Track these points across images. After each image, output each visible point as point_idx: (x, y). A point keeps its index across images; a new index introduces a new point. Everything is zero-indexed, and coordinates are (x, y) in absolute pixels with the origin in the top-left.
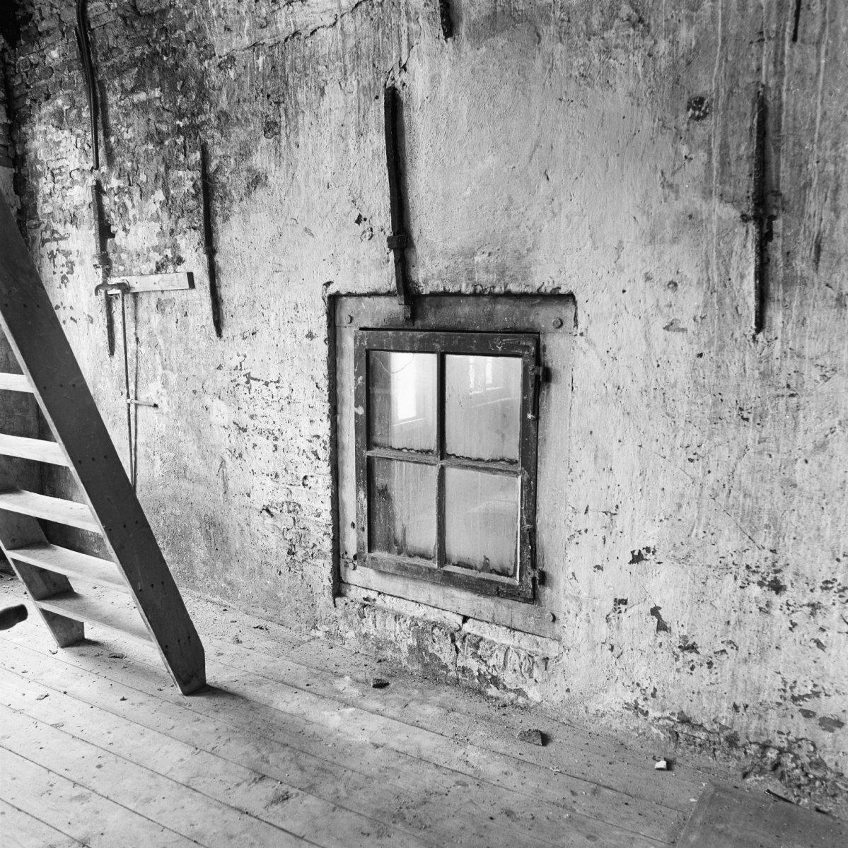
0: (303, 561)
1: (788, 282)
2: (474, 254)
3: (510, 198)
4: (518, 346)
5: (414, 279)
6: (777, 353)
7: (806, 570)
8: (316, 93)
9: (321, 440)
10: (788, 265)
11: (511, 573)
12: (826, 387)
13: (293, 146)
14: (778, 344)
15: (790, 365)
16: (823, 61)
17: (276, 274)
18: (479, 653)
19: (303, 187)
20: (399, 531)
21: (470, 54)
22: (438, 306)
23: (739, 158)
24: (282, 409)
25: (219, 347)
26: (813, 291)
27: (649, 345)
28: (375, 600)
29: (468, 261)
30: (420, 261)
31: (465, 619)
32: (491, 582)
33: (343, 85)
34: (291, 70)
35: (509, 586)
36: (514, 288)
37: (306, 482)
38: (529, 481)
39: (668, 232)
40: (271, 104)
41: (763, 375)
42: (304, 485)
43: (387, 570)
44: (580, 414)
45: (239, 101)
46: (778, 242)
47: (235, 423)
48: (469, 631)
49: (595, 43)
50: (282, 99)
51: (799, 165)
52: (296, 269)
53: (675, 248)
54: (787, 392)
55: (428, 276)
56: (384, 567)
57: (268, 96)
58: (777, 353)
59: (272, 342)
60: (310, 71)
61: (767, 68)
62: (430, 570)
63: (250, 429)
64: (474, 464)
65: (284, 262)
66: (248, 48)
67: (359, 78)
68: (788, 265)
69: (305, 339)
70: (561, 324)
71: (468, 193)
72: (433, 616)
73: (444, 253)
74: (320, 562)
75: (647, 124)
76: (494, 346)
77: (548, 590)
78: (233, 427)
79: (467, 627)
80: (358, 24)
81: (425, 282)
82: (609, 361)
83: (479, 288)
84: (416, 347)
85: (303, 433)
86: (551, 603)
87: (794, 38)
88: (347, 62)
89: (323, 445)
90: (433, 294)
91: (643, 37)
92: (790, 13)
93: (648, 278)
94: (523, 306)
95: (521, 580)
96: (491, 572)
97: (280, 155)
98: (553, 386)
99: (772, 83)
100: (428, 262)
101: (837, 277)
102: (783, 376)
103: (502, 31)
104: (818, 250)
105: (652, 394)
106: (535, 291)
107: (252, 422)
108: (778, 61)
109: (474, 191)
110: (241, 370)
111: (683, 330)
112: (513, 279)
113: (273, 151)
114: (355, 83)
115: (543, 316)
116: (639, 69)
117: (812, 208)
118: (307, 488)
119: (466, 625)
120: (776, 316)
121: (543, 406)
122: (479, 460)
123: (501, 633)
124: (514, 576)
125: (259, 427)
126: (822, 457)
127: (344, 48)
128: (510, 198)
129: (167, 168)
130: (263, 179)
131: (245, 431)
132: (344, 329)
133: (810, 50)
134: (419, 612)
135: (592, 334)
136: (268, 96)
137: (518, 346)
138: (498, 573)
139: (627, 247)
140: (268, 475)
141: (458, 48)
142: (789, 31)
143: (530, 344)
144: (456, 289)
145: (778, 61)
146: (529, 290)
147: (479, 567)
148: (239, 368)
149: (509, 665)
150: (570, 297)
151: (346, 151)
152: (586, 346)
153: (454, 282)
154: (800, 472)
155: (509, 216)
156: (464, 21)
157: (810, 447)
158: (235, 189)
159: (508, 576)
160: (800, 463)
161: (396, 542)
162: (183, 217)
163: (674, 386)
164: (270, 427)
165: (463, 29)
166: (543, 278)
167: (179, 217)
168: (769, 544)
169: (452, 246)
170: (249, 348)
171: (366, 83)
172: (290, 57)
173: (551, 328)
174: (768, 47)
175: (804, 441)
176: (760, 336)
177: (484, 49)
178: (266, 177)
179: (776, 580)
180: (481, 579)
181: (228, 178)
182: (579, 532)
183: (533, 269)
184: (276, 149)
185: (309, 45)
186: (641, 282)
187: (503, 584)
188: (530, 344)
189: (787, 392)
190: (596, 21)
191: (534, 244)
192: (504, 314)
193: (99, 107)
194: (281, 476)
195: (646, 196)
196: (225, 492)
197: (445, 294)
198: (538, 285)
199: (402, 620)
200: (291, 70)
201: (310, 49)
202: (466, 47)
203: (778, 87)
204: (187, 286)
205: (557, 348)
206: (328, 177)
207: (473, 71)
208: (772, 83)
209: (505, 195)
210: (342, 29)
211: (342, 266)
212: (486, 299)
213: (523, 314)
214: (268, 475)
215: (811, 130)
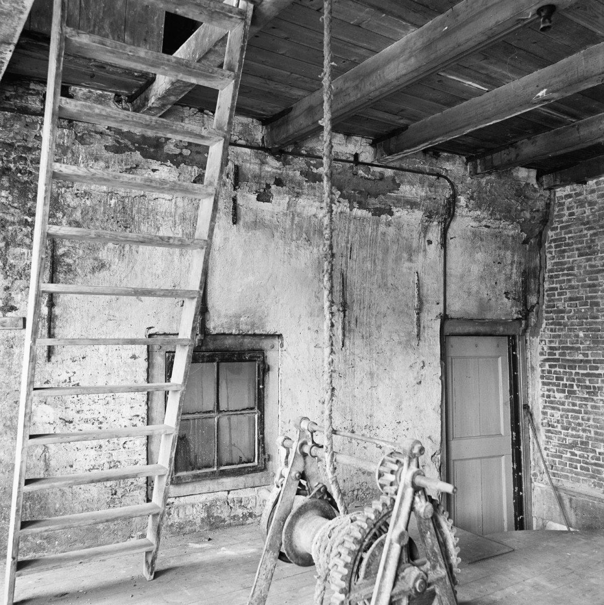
0: (122, 496)
1: (350, 331)
2: (241, 317)
3: (259, 295)
4: (256, 357)
5: (208, 326)
6: (348, 354)
7: (360, 424)
8: (155, 229)
9: (140, 418)
10: (349, 326)
11: (252, 461)
12: (361, 363)
13: (134, 252)
14: (348, 351)
15: (351, 357)
16: (121, 51)
17: (109, 322)
18: (242, 504)
19: (139, 275)
20: (192, 457)
21: (244, 234)
22: (215, 340)
23: (337, 291)
24: (108, 403)
25: (47, 368)
26: (356, 334)
27: (309, 353)
28: (173, 503)
29: (237, 319)
30: (212, 318)
31: (229, 492)
32: (244, 468)
33: (173, 229)
34: (138, 213)
35: (253, 467)
36: (257, 332)
37: (125, 445)
38: (261, 415)
39: (316, 313)
40: (120, 226)
41: (345, 361)
42: (124, 448)
43: (187, 481)
44: (285, 382)
45: (92, 219)
46: (347, 318)
47: (60, 419)
48: (232, 497)
49: (293, 243)
50: (128, 226)
51: (351, 296)
52: (127, 319)
53: (318, 319)
54: (351, 366)
55: (215, 324)
56: (185, 479)
57: (118, 222)
58: (348, 354)
59: (101, 362)
60: (151, 217)
61: (344, 265)
62: (213, 473)
63: (76, 420)
64: (235, 413)
65: (117, 314)
66: (104, 192)
67: (184, 228)
68: (349, 326)
69: (129, 359)
70: (273, 347)
71: (240, 290)
72: (211, 497)
73: (226, 316)
74: (136, 493)
75: (310, 275)
76: (245, 357)
77: (270, 462)
78: (59, 422)
79: (231, 496)
80: (185, 205)
81: (214, 328)
82: (296, 361)
83: (241, 332)
84: (205, 359)
85: (123, 416)
86: (272, 468)
87: (350, 258)
88: (177, 219)
89: (142, 420)
90: (217, 334)
91: (309, 246)
92: (349, 251)
93: (309, 329)
94: (257, 339)
95: (258, 462)
96: (243, 463)
97: (123, 255)
98: (270, 372)
99: (345, 269)
100: (216, 319)
101: (361, 330)
102: (350, 361)
103: (259, 229)
104: (357, 322)
105: (311, 371)
106: (266, 333)
107: (78, 415)
108: (346, 263)
109: (243, 290)
110: (70, 382)
111: (320, 347)
112: (258, 328)
113: (118, 252)
114: (180, 230)
115: (265, 344)
116: (308, 256)
117: (355, 309)
118: (127, 450)
119: (230, 495)
120: (347, 342)
121: (266, 380)
122: (236, 411)
123: (248, 492)
124: (254, 461)
125: (84, 418)
126: (361, 386)
127: (175, 212)
128: (259, 295)
129: (7, 245)
130: (108, 266)
131: (71, 422)
132: (154, 353)
133: (354, 263)
134: (203, 498)
135: (289, 350)
136: (118, 222)
137: (256, 357)
138: (246, 463)
139: (303, 317)
140: (92, 448)
141: (239, 230)
142: (349, 256)
143: (261, 355)
144: (230, 332)
145: (346, 263)
146: (264, 333)
147: (236, 463)
148: (68, 380)
149: (258, 504)
150: (280, 336)
151: (172, 261)
152: (287, 355)
153: (229, 329)
154: (356, 392)
155: (258, 302)
156: (242, 220)
157: (358, 383)
158: (81, 268)
159: (251, 462)
160: (356, 390)
161: (191, 464)
162: (21, 279)
163: (318, 368)
164: (95, 416)
165: (241, 223)
166: (270, 329)
167: (16, 279)
168: (350, 418)
169: (231, 312)
170: (79, 367)
171: (188, 232)
172: (137, 206)
173: (269, 348)
174: (344, 259)
175: (357, 381)
176: (343, 349)
177: (250, 234)
178: (110, 266)
179: (352, 430)
180: (239, 468)
181: (75, 261)
182: (287, 431)
183: (266, 324)
184: (121, 251)
185: (152, 204)
186: (307, 330)
187: (250, 467)
188: (261, 355)
189: (351, 366)
190: (294, 237)
191: (268, 314)
192: (248, 343)
193: (464, 357)
194: (104, 447)
195: (310, 300)
196: (47, 470)
197: (224, 334)
198: (268, 331)
199: (196, 506)
200: (138, 213)
201: (152, 206)
202: (243, 230)
203: (347, 271)
204: (22, 327)
205: (272, 357)
206: (159, 272)
207: (245, 241)
208: (345, 269)
209: (257, 293)
210: (175, 203)
211: (161, 319)
212: (239, 336)
213: (259, 343)
214: (92, 448)
215: (354, 285)
